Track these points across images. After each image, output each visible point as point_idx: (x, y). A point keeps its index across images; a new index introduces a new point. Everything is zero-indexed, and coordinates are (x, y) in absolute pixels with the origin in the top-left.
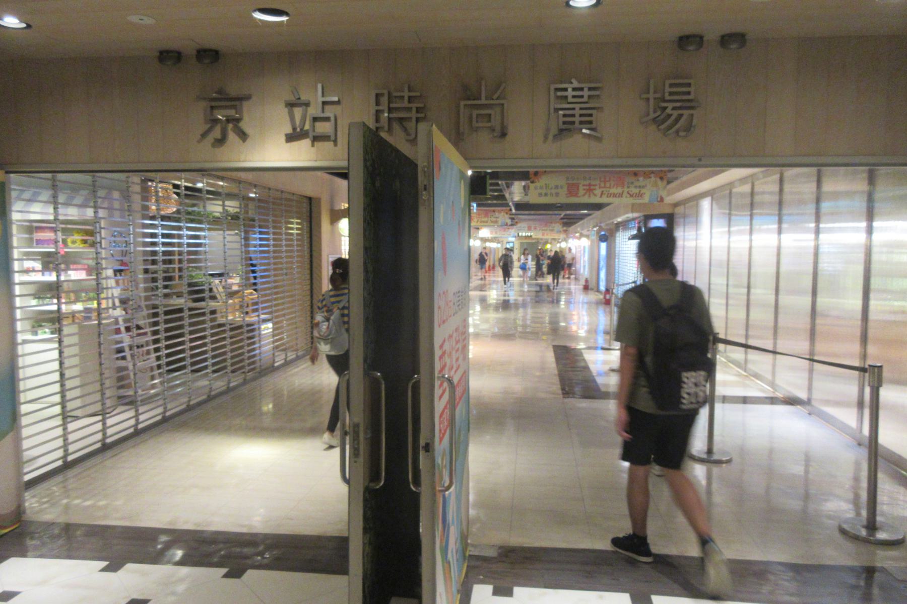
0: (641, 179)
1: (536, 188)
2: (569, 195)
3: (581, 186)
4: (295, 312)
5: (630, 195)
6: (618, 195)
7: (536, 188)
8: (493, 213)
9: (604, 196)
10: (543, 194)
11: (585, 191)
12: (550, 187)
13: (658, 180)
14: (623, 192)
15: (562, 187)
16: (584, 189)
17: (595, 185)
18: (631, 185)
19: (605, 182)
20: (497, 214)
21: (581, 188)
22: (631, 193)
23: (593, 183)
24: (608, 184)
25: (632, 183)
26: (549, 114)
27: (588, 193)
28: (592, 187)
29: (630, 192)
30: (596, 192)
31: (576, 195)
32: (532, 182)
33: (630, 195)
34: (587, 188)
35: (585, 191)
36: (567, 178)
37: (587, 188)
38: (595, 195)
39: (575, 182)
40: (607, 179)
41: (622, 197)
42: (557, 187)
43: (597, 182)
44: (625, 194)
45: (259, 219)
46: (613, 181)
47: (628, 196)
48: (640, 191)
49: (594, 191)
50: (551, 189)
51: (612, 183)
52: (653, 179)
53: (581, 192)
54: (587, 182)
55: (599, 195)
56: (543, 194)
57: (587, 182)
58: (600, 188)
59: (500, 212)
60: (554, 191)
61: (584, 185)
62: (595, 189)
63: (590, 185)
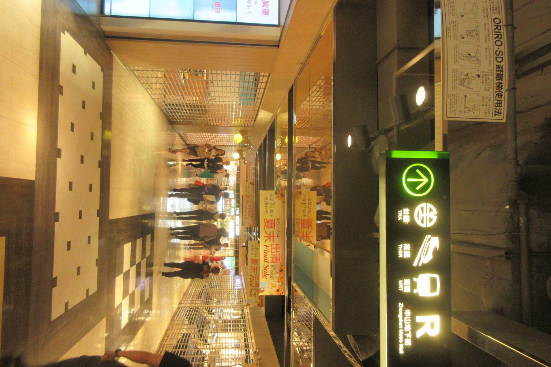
0: (278, 275)
1: (271, 195)
2: (266, 221)
3: (256, 265)
4: (231, 287)
5: (266, 267)
6: (265, 258)
7: (271, 195)
8: (251, 216)
9: (251, 277)
10: (267, 201)
11: (269, 233)
12: (272, 206)
13: (258, 303)
14: (269, 262)
15: (256, 256)
16: (254, 267)
17: (256, 273)
18: (273, 268)
19: (276, 248)
20: (251, 219)
21: (272, 230)
22: (267, 269)
23: (275, 238)
24: (274, 250)
25: (275, 269)
26: (493, 45)
27: (252, 269)
28: (272, 238)
29: (268, 267)
30: (253, 273)
31: (266, 226)
32: (276, 193)
33: (266, 267)
34: (272, 235)
35: (269, 233)
36: (279, 219)
37: (255, 269)
38: (251, 273)
39: (276, 225)
40: (278, 250)
41: (264, 261)
42: (272, 211)
43: (275, 242)
44: (252, 288)
45: (250, 105)
46: (277, 255)
47: (265, 266)
48: (269, 275)
49: (268, 240)
50: (271, 207)
51: (275, 254)
52: (259, 301)
53: (268, 230)
54: (275, 234)
55: (266, 244)
56: (267, 201)
57: (275, 234)
58: (272, 245)
59: (252, 220)
60: (269, 209)
61: (273, 232)
62: (254, 272)
63: (273, 237)
